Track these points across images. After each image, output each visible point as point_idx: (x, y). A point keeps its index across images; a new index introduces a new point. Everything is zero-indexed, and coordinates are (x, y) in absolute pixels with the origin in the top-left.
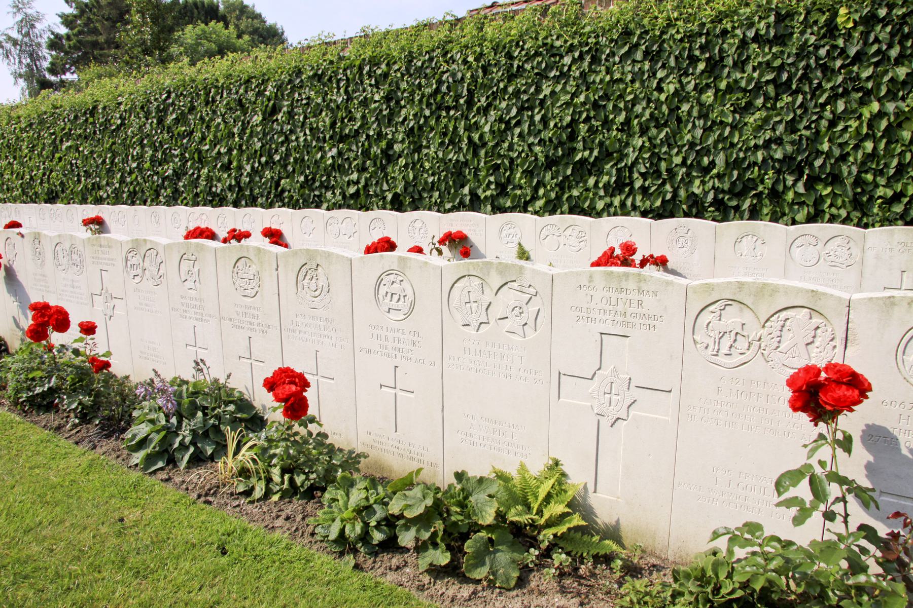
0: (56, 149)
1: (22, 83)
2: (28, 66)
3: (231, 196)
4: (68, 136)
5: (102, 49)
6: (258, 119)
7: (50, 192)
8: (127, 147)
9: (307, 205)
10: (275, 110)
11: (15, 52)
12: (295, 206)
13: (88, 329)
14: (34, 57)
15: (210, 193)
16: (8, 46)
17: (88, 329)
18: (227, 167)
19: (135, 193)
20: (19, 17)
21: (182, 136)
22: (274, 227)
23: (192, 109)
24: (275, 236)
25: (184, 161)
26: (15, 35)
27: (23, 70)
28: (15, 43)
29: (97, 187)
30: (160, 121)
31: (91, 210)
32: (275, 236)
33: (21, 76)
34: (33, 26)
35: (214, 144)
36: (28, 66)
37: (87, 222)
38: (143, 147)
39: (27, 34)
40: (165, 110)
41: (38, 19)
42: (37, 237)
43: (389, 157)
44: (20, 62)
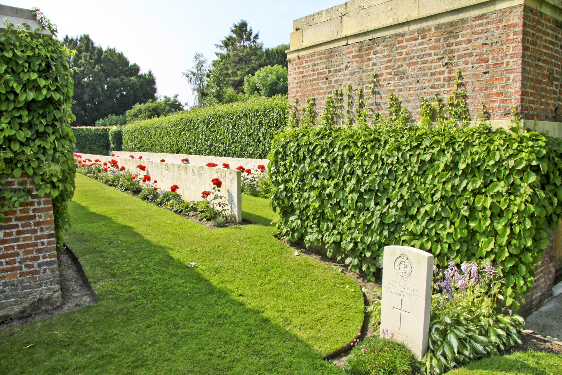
0: (180, 134)
1: (196, 93)
2: (199, 85)
3: (224, 153)
4: (184, 129)
5: (230, 77)
6: (231, 127)
7: (178, 149)
8: (199, 135)
9: (241, 157)
10: (235, 125)
11: (194, 78)
12: (239, 157)
13: (156, 182)
14: (202, 81)
15: (219, 152)
16: (191, 76)
17: (156, 182)
18: (223, 143)
19: (200, 151)
20: (197, 63)
21: (213, 132)
22: (226, 163)
23: (216, 123)
24: (226, 166)
25: (213, 140)
26: (195, 71)
27: (197, 87)
28: (194, 75)
29: (190, 148)
30: (207, 126)
31: (185, 156)
32: (226, 166)
33: (195, 90)
34: (202, 66)
35: (220, 135)
36: (199, 85)
37: (183, 161)
38: (202, 135)
39: (200, 70)
40: (209, 123)
41: (204, 62)
42: (152, 162)
43: (259, 141)
44: (196, 83)
